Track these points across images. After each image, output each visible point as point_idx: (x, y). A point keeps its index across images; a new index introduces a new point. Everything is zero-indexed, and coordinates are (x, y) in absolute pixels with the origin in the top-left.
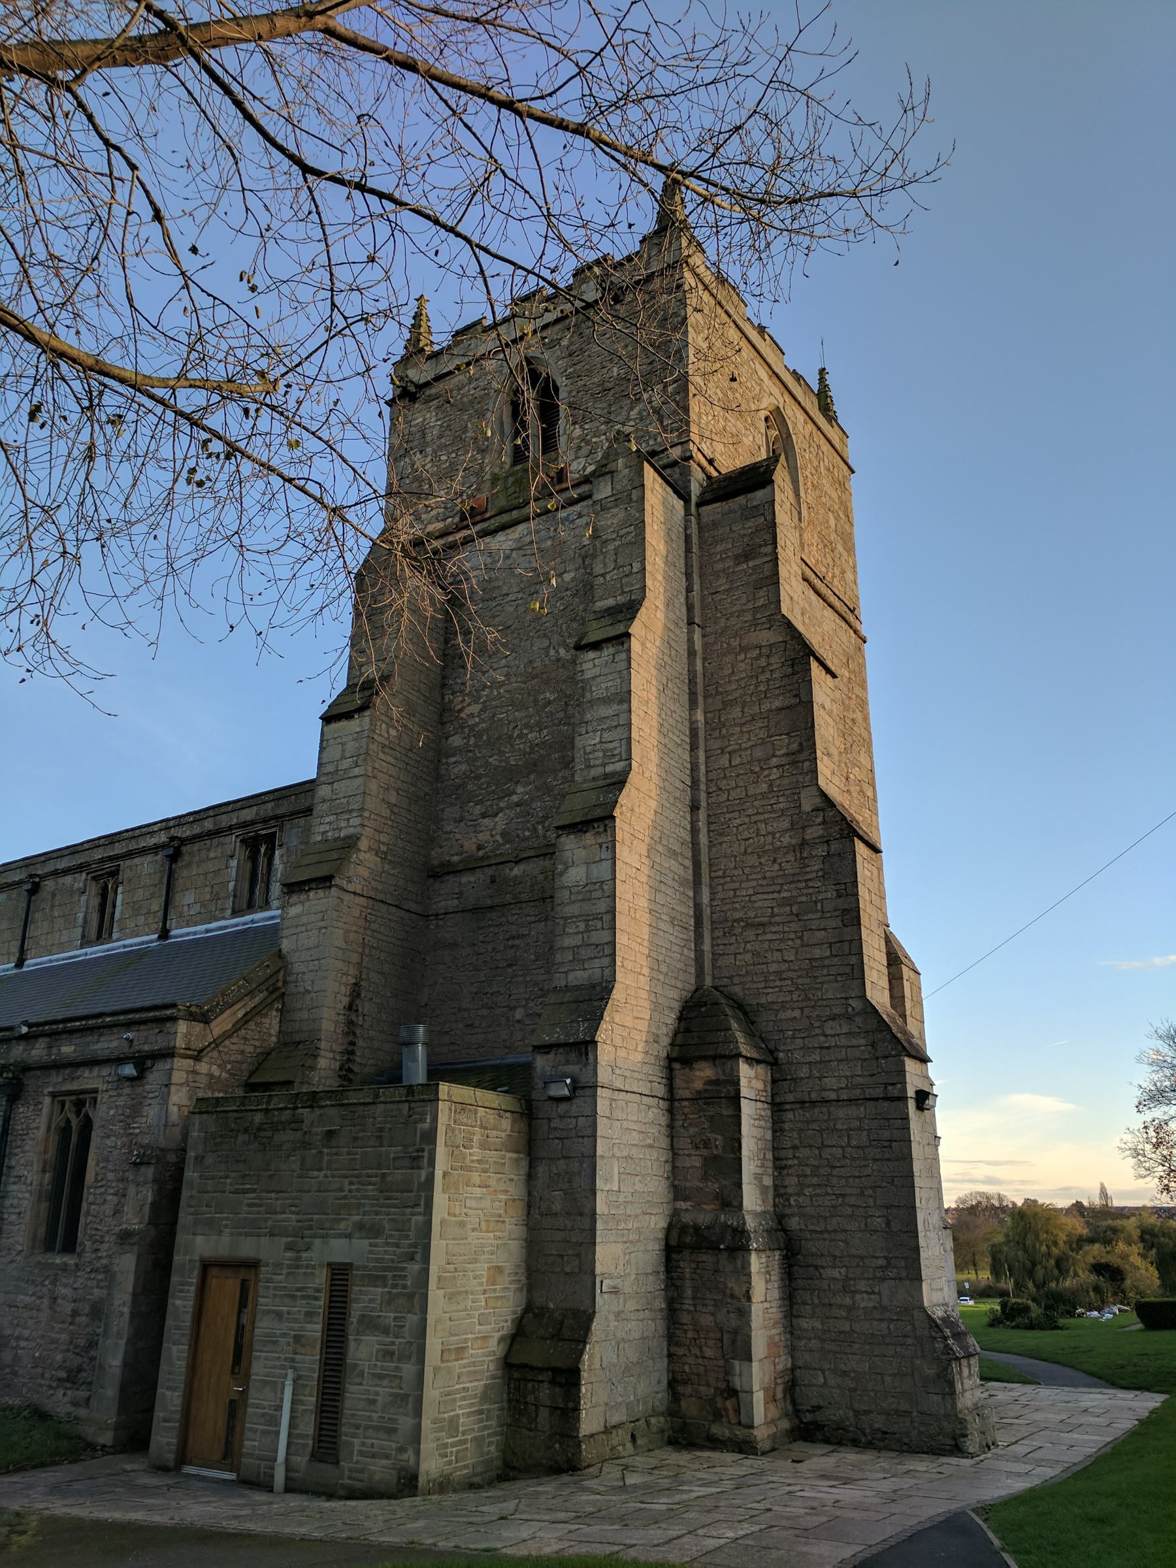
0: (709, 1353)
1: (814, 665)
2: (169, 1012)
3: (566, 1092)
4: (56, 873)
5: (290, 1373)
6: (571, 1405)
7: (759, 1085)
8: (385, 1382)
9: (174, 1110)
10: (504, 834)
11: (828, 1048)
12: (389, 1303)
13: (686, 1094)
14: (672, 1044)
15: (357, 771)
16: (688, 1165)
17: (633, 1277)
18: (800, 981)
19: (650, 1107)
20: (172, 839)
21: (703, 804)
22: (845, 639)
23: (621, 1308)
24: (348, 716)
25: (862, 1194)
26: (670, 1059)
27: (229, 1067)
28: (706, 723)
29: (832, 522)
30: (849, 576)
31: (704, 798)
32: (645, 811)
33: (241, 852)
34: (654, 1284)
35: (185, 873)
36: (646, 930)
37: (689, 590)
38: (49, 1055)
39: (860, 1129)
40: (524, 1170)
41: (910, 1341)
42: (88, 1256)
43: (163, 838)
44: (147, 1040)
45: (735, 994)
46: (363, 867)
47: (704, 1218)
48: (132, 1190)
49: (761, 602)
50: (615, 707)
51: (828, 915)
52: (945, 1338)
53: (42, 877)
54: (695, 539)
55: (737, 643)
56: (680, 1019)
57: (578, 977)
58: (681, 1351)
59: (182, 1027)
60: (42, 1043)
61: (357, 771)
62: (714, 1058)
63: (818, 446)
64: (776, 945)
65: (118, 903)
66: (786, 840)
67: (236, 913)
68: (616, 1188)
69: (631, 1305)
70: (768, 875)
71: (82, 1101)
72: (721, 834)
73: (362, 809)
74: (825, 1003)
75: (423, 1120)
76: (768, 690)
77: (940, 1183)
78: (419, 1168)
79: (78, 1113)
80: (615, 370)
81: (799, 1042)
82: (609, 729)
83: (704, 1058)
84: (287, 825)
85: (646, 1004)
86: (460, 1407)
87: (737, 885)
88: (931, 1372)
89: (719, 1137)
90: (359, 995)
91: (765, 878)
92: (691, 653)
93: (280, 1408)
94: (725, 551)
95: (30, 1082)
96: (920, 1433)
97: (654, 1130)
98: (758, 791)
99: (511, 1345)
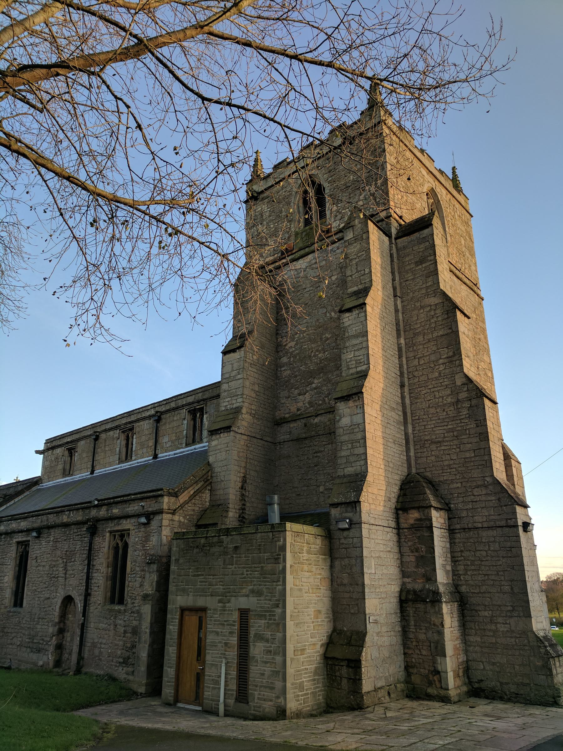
0: (424, 653)
1: (458, 313)
2: (159, 493)
3: (347, 526)
4: (106, 431)
5: (224, 660)
6: (358, 677)
7: (442, 521)
8: (268, 665)
9: (164, 538)
10: (310, 403)
11: (476, 502)
12: (268, 627)
13: (406, 526)
14: (397, 502)
15: (239, 377)
16: (408, 560)
17: (385, 615)
18: (460, 469)
19: (388, 532)
20: (157, 412)
21: (407, 384)
22: (473, 299)
23: (379, 630)
24: (234, 351)
25: (498, 574)
26: (397, 509)
27: (188, 517)
28: (406, 344)
29: (463, 242)
30: (473, 268)
31: (407, 381)
32: (377, 389)
33: (188, 417)
34: (395, 619)
35: (163, 428)
36: (382, 446)
37: (394, 280)
38: (108, 514)
39: (494, 541)
40: (328, 564)
41: (527, 648)
42: (130, 606)
43: (152, 412)
44: (150, 506)
45: (428, 477)
46: (245, 422)
47: (418, 586)
48: (147, 575)
49: (430, 283)
50: (360, 339)
51: (472, 436)
52: (546, 647)
53: (100, 433)
54: (395, 255)
55: (419, 304)
56: (401, 489)
57: (349, 470)
58: (410, 652)
59: (166, 499)
60: (104, 508)
61: (239, 377)
62: (418, 508)
63: (454, 205)
64: (447, 452)
65: (134, 443)
66: (449, 400)
67: (187, 445)
68: (374, 572)
69: (384, 629)
70: (441, 417)
71: (123, 535)
72: (416, 398)
73: (243, 394)
74: (473, 479)
75: (279, 541)
76: (436, 328)
77: (364, 588)
78: (279, 563)
79: (122, 540)
80: (351, 177)
81: (461, 499)
82: (358, 350)
83: (414, 508)
84: (209, 403)
85: (384, 483)
86: (305, 677)
87: (425, 423)
88: (539, 664)
89: (423, 546)
90: (246, 482)
91: (439, 419)
92: (397, 311)
93: (220, 676)
94: (410, 260)
95: (100, 526)
96: (535, 695)
97: (391, 544)
98: (434, 376)
99: (327, 648)
